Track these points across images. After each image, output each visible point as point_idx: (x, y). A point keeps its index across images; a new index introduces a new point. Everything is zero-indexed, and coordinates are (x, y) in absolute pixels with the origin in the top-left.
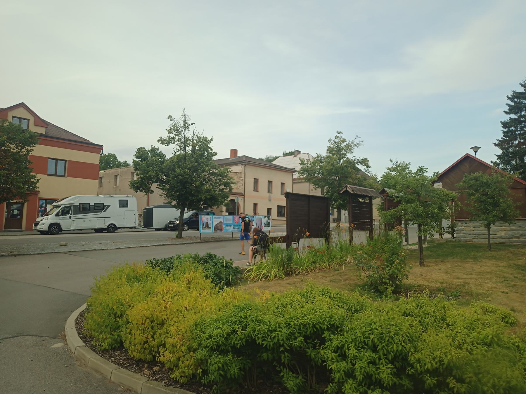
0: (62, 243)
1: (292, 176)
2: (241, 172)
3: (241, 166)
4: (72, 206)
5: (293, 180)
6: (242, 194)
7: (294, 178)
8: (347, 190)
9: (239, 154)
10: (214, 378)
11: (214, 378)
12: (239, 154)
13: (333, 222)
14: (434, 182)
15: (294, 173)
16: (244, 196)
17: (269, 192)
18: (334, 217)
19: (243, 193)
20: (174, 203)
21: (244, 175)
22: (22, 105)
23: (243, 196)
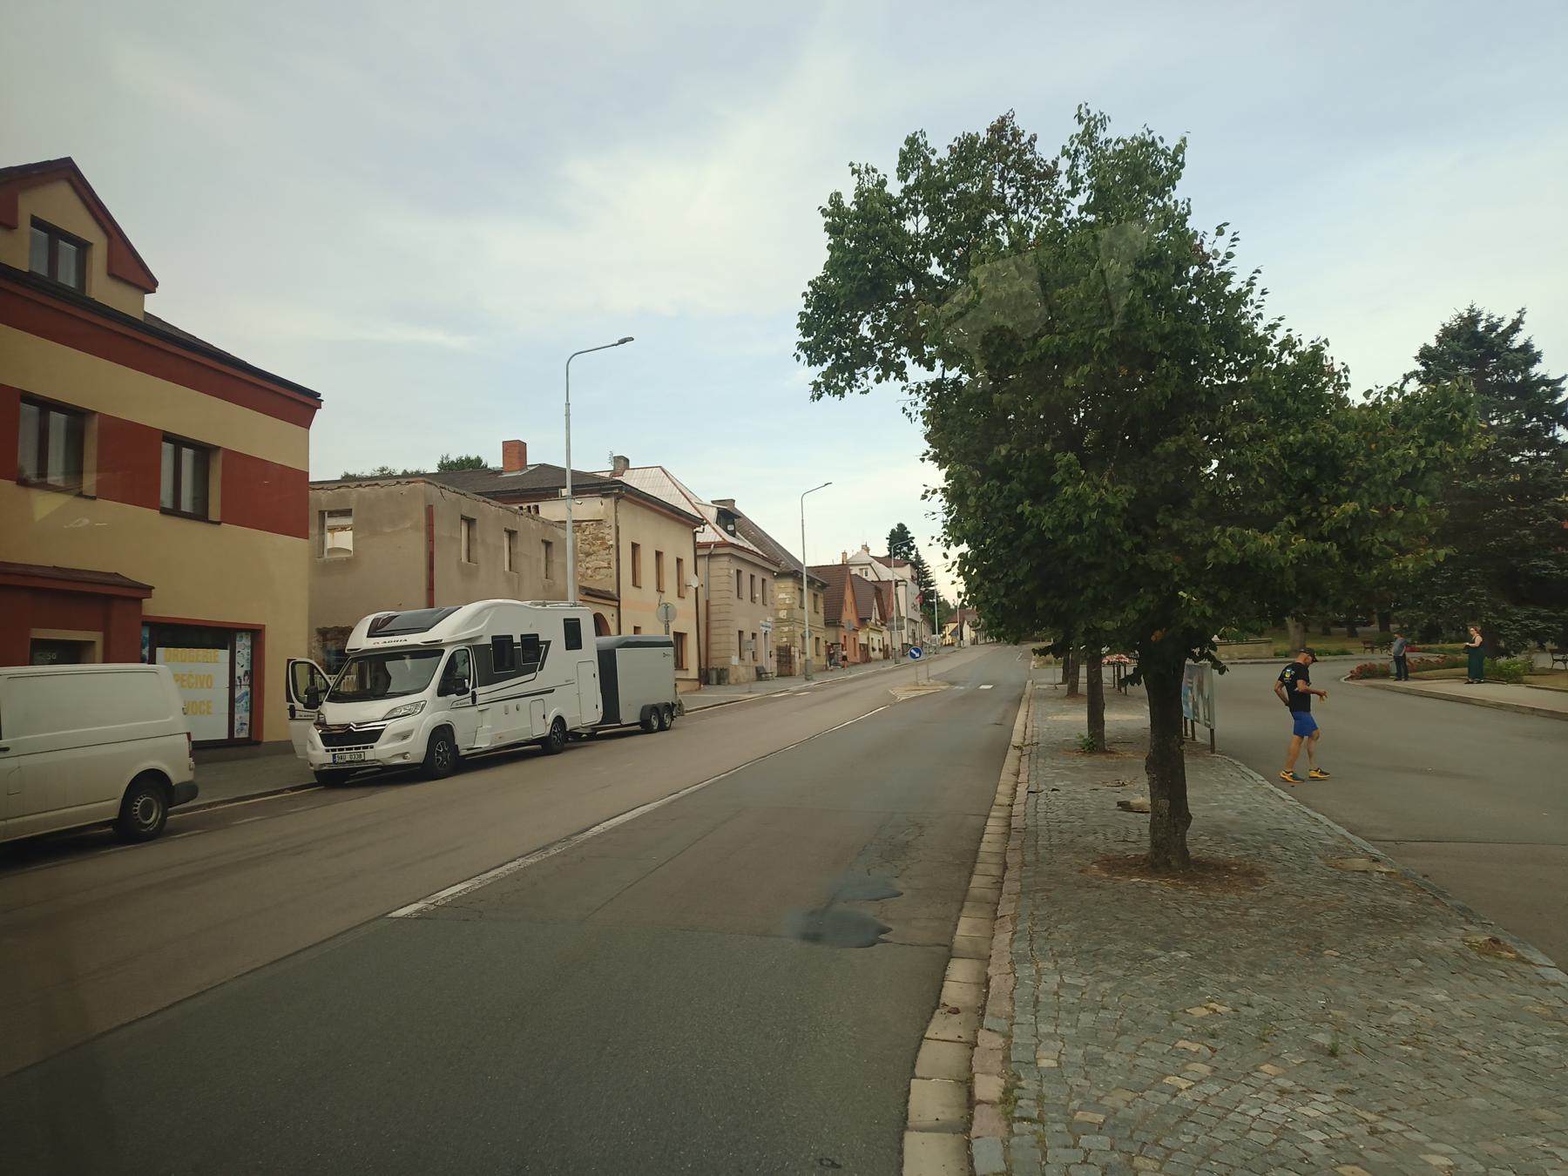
0: (444, 894)
1: (692, 536)
2: (599, 521)
3: (600, 499)
4: (469, 647)
5: (698, 546)
6: (613, 595)
7: (697, 540)
8: (565, 599)
9: (533, 459)
10: (1026, 361)
11: (1026, 361)
12: (533, 459)
13: (758, 680)
14: (145, 624)
15: (697, 529)
16: (619, 601)
17: (658, 590)
18: (757, 665)
19: (615, 592)
20: (855, 571)
21: (613, 531)
22: (64, 171)
23: (617, 604)
